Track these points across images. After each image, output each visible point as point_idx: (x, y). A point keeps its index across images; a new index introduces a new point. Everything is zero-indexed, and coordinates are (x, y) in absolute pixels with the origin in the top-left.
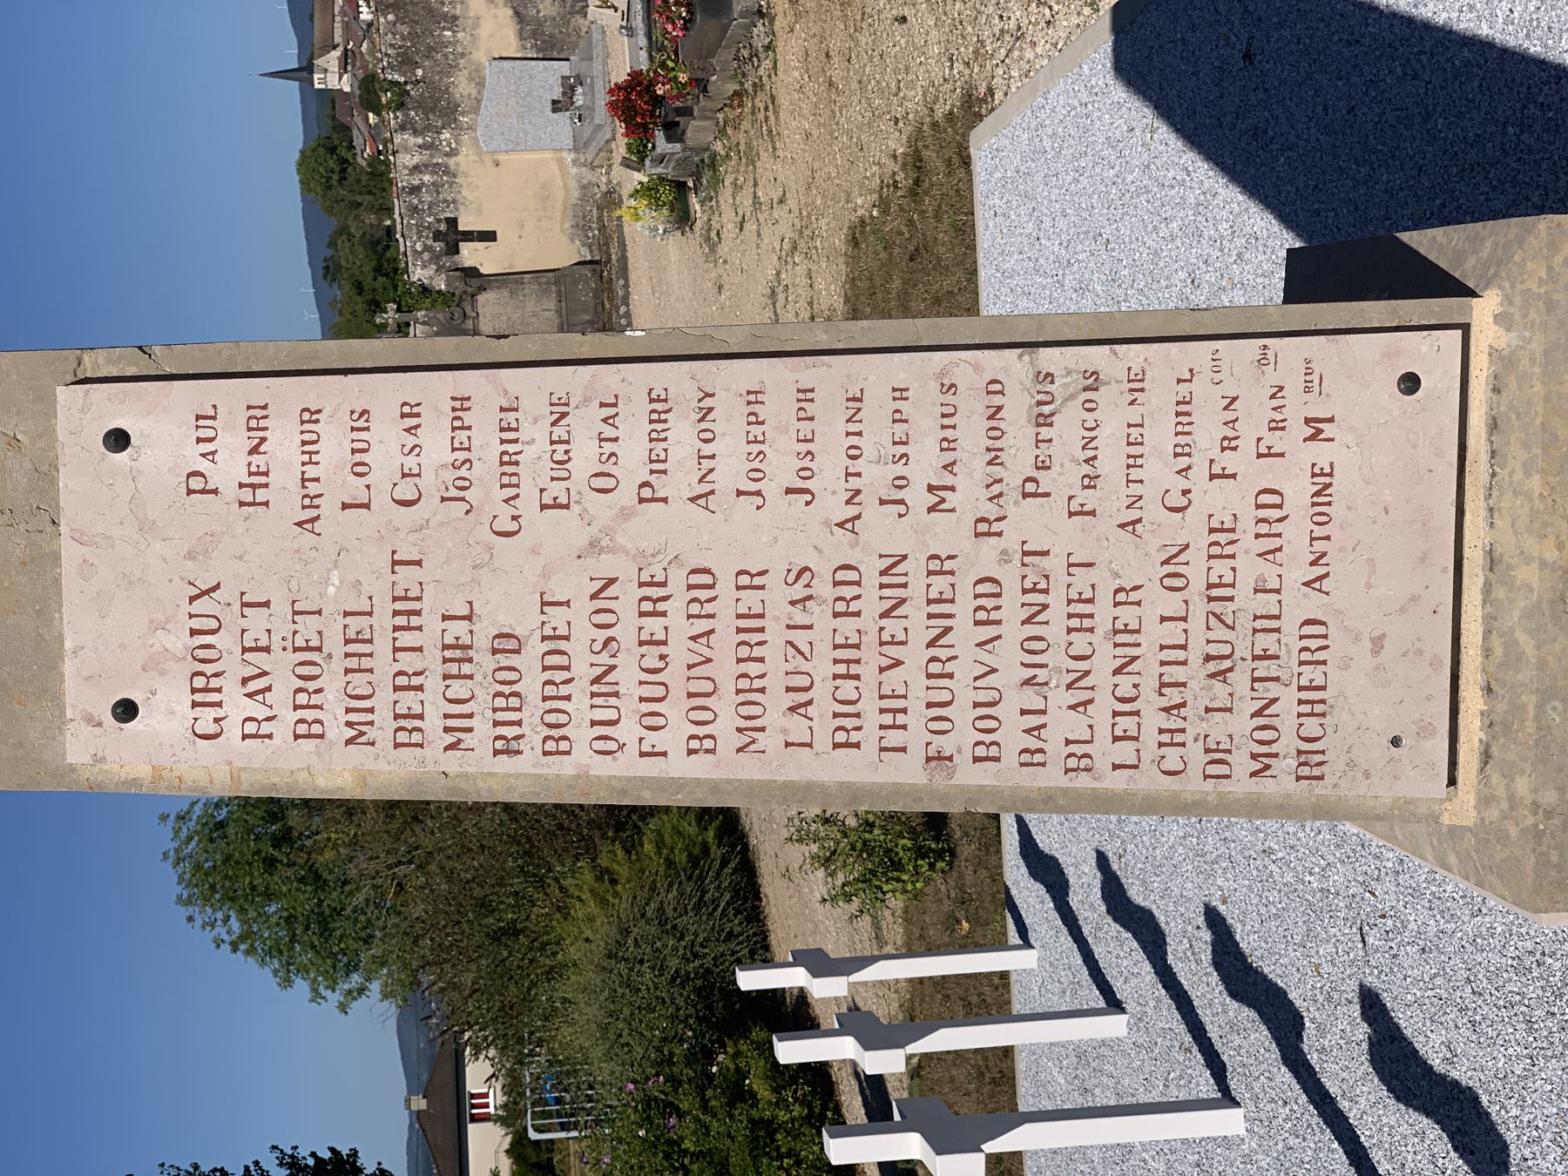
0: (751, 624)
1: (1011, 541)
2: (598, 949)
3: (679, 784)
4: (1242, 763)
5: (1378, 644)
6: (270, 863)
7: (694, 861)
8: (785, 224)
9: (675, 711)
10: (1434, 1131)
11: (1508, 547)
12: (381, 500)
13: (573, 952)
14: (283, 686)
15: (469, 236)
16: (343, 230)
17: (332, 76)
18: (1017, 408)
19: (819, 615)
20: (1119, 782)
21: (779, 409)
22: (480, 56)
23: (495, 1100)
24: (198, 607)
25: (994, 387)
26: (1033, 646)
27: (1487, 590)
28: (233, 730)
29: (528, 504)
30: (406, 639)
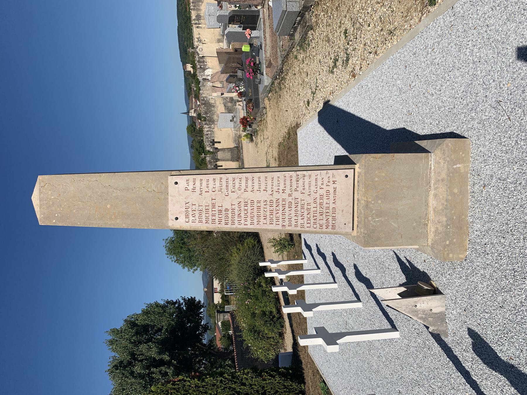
0: (259, 208)
1: (293, 197)
2: (237, 261)
3: (249, 229)
4: (324, 227)
5: (343, 211)
6: (181, 247)
7: (253, 247)
8: (269, 142)
9: (249, 219)
10: (364, 286)
11: (360, 198)
12: (210, 191)
13: (233, 262)
14: (197, 215)
15: (216, 142)
16: (194, 140)
17: (192, 114)
18: (294, 179)
19: (268, 207)
20: (308, 229)
21: (263, 179)
22: (218, 112)
23: (219, 289)
24: (186, 205)
25: (291, 177)
26: (296, 211)
27: (357, 204)
28: (191, 221)
29: (230, 192)
30: (213, 209)
